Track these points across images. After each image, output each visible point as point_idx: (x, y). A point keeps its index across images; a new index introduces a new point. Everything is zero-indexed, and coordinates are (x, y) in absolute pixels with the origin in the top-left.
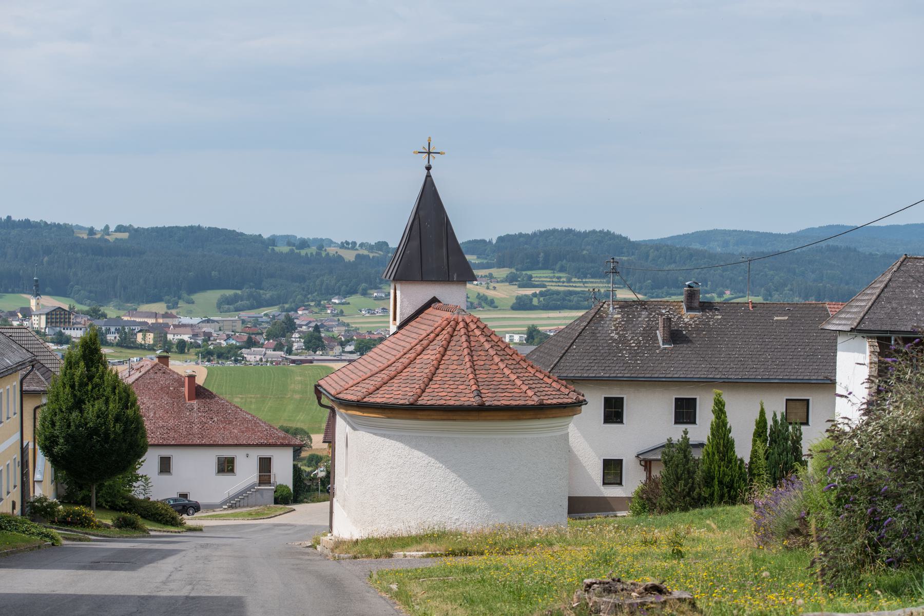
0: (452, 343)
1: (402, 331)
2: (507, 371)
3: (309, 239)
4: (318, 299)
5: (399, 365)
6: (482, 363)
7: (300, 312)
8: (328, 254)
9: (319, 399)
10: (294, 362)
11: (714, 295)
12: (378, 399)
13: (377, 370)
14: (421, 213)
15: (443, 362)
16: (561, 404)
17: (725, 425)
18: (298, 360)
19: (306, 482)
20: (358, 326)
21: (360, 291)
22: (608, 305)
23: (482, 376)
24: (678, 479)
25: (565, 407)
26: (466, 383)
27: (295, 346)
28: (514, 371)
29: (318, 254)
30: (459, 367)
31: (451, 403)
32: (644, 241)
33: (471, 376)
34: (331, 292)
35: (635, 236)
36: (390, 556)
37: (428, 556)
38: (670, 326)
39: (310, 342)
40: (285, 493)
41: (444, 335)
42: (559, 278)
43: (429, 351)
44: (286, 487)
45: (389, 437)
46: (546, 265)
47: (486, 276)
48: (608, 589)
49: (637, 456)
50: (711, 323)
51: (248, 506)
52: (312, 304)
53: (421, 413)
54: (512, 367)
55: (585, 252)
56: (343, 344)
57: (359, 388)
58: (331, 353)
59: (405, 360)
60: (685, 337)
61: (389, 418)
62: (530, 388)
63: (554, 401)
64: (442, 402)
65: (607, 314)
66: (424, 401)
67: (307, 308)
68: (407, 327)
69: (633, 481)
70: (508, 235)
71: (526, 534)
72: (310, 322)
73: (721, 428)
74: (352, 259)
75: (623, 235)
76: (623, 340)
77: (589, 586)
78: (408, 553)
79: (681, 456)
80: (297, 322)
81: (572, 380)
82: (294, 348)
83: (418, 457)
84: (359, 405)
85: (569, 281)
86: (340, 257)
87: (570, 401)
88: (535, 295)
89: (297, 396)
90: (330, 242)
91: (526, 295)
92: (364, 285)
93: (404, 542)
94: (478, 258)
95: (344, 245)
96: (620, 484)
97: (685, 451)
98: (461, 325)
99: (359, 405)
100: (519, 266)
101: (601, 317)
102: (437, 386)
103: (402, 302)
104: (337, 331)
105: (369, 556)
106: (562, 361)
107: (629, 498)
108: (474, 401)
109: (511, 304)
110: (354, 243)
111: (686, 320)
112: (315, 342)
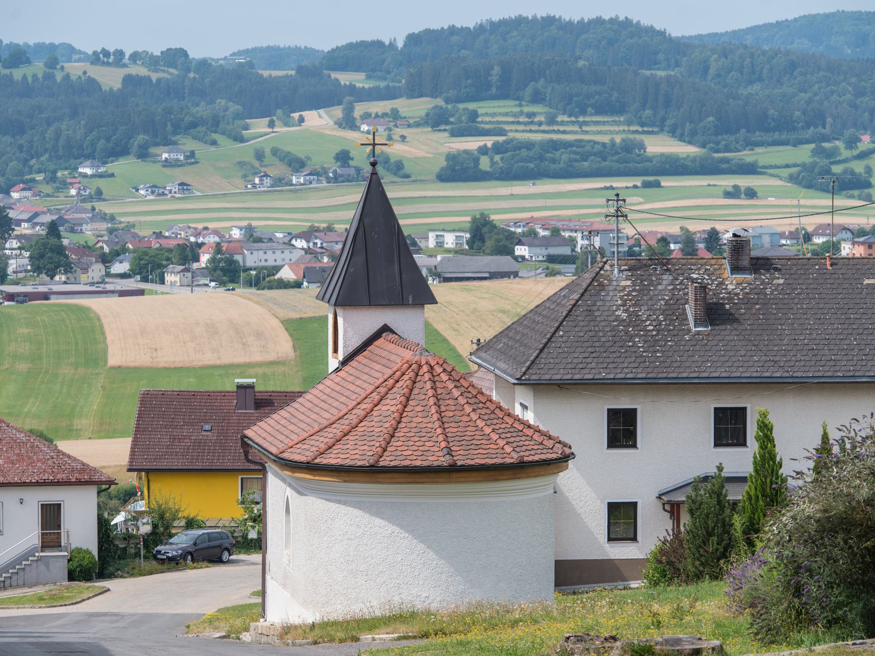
0: (415, 391)
1: (347, 368)
2: (480, 423)
3: (27, 45)
4: (52, 167)
5: (353, 418)
6: (451, 414)
7: (15, 195)
8: (67, 77)
9: (246, 454)
10: (11, 297)
11: (840, 144)
12: (331, 459)
13: (326, 423)
14: (367, 221)
15: (405, 414)
16: (544, 460)
17: (773, 457)
18: (19, 294)
19: (117, 543)
20: (131, 219)
21: (134, 149)
22: (612, 266)
23: (451, 430)
24: (710, 534)
25: (549, 464)
26: (434, 439)
27: (13, 265)
28: (489, 422)
29: (49, 77)
30: (425, 420)
31: (418, 463)
32: (700, 37)
33: (439, 431)
34: (77, 153)
35: (678, 27)
36: (357, 640)
37: (399, 639)
38: (705, 298)
39: (42, 256)
40: (85, 562)
41: (405, 382)
42: (531, 115)
43: (388, 401)
44: (88, 552)
45: (345, 503)
46: (506, 90)
47: (385, 115)
48: (579, 639)
49: (659, 497)
50: (768, 291)
51: (24, 585)
52: (40, 177)
53: (383, 476)
54: (486, 417)
55: (581, 63)
56: (106, 260)
57: (305, 446)
58: (84, 278)
59: (359, 412)
60: (729, 314)
61: (345, 481)
62: (507, 443)
63: (536, 458)
64: (407, 463)
65: (611, 281)
66: (387, 461)
67: (29, 185)
68: (353, 363)
69: (654, 530)
70: (428, 32)
71: (508, 612)
72: (36, 215)
73: (768, 462)
74: (117, 85)
75: (658, 27)
76: (635, 320)
77: (568, 638)
78: (377, 636)
79: (714, 501)
80: (12, 214)
81: (559, 385)
82: (10, 270)
83: (380, 526)
84: (310, 467)
85: (552, 121)
86: (92, 82)
87: (554, 456)
88: (483, 150)
89: (23, 367)
90: (70, 50)
91: (466, 152)
92: (141, 138)
93: (372, 624)
94: (369, 77)
95: (100, 58)
96: (634, 539)
97: (719, 495)
98: (425, 368)
99: (310, 467)
100: (452, 93)
101: (601, 285)
102: (400, 443)
103: (345, 332)
104: (89, 232)
105: (332, 640)
106: (543, 355)
107: (647, 560)
108: (444, 461)
109: (436, 169)
110: (120, 54)
111: (730, 287)
112: (51, 256)
